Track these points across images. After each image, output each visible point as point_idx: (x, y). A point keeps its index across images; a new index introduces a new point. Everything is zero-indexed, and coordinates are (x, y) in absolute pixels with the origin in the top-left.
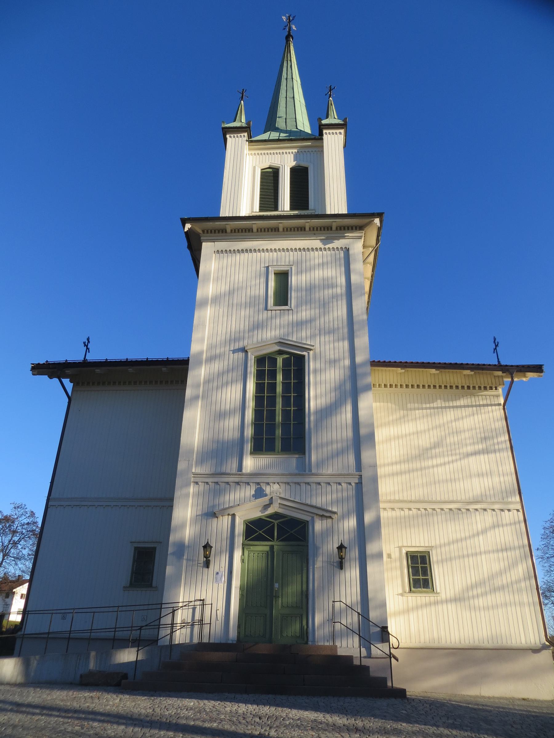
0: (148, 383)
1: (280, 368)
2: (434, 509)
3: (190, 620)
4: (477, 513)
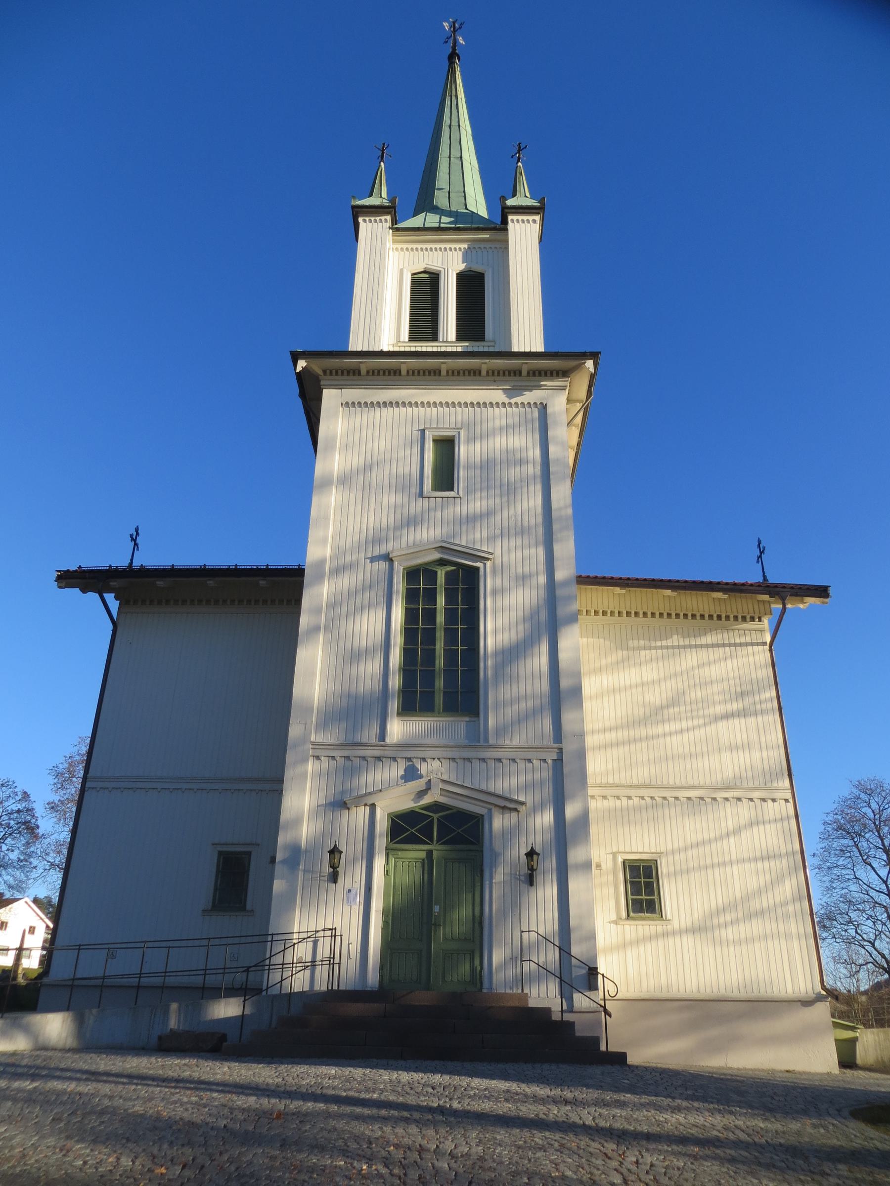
0: (236, 602)
1: (441, 585)
2: (665, 798)
3: (309, 959)
4: (728, 804)
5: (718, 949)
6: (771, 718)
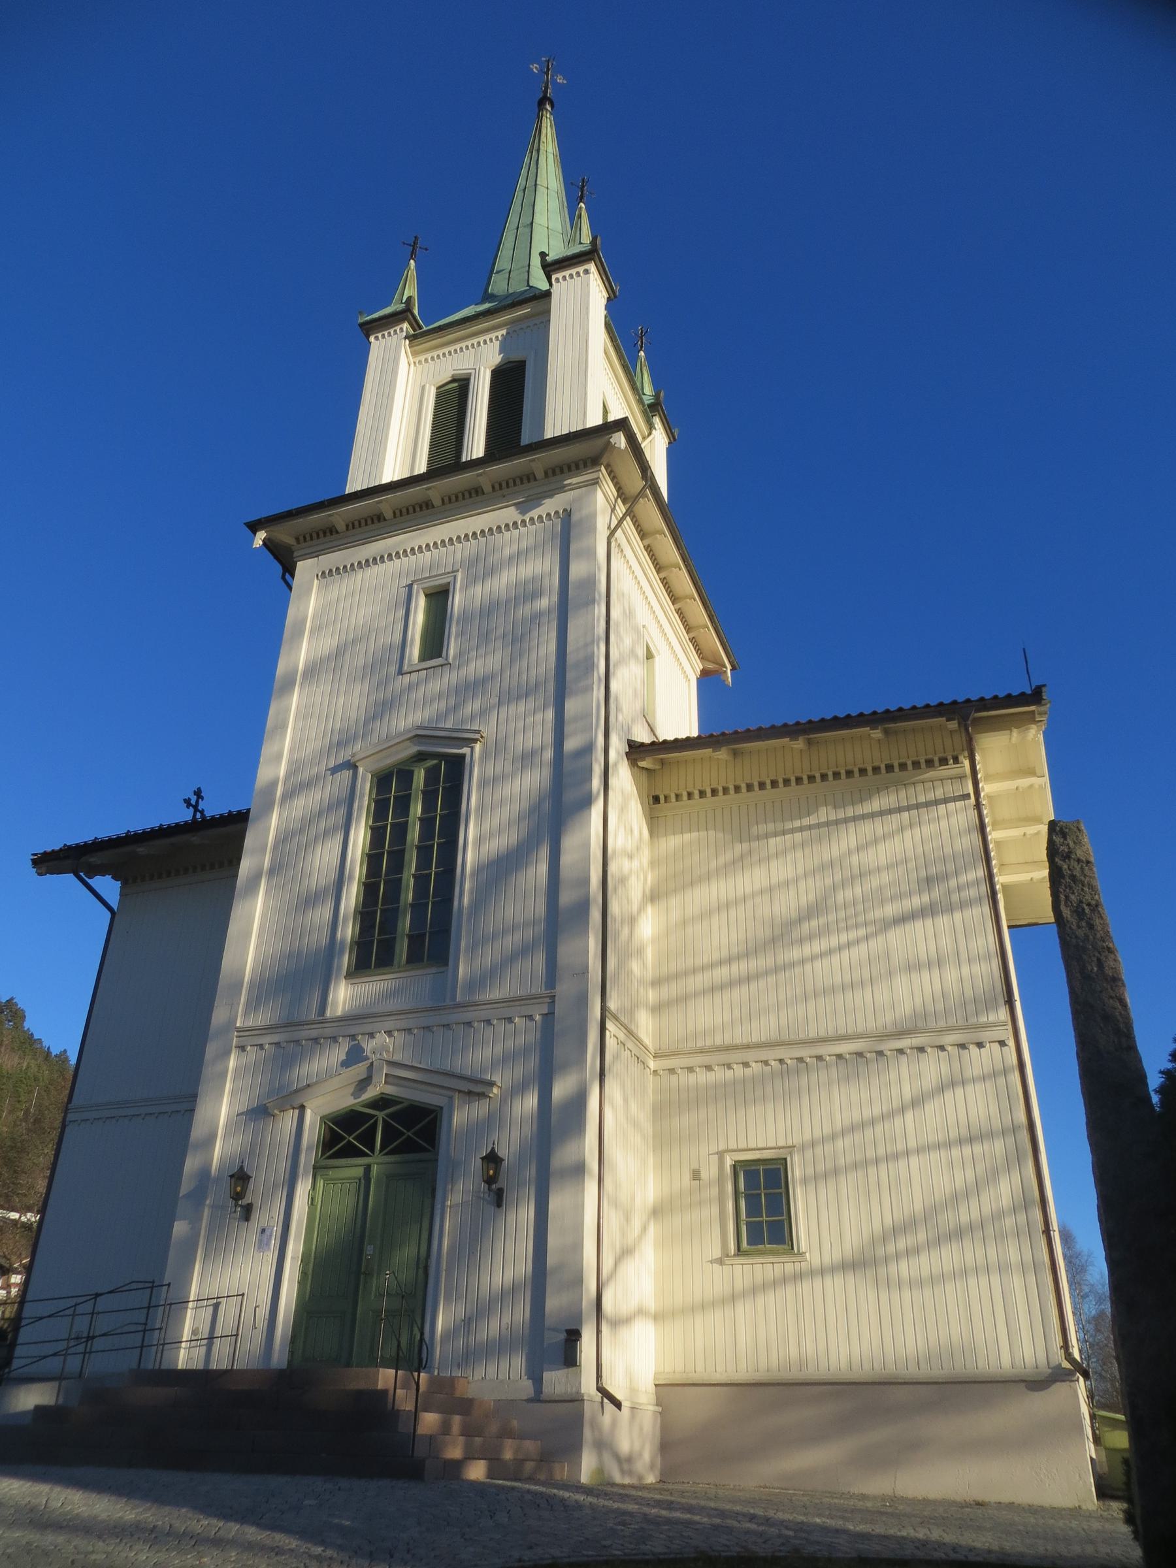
2: (800, 1060)
4: (903, 1059)
5: (884, 1296)
6: (976, 911)
